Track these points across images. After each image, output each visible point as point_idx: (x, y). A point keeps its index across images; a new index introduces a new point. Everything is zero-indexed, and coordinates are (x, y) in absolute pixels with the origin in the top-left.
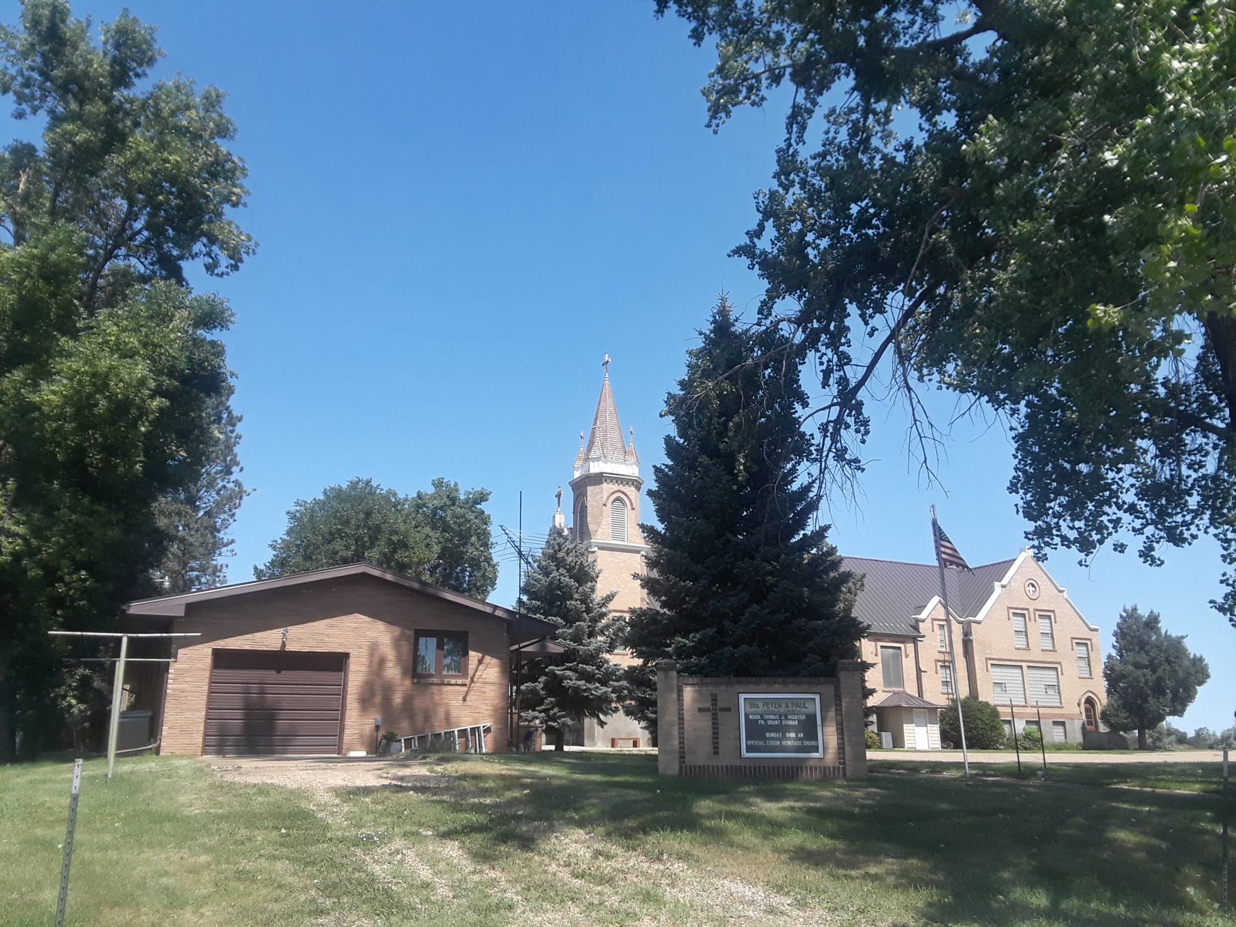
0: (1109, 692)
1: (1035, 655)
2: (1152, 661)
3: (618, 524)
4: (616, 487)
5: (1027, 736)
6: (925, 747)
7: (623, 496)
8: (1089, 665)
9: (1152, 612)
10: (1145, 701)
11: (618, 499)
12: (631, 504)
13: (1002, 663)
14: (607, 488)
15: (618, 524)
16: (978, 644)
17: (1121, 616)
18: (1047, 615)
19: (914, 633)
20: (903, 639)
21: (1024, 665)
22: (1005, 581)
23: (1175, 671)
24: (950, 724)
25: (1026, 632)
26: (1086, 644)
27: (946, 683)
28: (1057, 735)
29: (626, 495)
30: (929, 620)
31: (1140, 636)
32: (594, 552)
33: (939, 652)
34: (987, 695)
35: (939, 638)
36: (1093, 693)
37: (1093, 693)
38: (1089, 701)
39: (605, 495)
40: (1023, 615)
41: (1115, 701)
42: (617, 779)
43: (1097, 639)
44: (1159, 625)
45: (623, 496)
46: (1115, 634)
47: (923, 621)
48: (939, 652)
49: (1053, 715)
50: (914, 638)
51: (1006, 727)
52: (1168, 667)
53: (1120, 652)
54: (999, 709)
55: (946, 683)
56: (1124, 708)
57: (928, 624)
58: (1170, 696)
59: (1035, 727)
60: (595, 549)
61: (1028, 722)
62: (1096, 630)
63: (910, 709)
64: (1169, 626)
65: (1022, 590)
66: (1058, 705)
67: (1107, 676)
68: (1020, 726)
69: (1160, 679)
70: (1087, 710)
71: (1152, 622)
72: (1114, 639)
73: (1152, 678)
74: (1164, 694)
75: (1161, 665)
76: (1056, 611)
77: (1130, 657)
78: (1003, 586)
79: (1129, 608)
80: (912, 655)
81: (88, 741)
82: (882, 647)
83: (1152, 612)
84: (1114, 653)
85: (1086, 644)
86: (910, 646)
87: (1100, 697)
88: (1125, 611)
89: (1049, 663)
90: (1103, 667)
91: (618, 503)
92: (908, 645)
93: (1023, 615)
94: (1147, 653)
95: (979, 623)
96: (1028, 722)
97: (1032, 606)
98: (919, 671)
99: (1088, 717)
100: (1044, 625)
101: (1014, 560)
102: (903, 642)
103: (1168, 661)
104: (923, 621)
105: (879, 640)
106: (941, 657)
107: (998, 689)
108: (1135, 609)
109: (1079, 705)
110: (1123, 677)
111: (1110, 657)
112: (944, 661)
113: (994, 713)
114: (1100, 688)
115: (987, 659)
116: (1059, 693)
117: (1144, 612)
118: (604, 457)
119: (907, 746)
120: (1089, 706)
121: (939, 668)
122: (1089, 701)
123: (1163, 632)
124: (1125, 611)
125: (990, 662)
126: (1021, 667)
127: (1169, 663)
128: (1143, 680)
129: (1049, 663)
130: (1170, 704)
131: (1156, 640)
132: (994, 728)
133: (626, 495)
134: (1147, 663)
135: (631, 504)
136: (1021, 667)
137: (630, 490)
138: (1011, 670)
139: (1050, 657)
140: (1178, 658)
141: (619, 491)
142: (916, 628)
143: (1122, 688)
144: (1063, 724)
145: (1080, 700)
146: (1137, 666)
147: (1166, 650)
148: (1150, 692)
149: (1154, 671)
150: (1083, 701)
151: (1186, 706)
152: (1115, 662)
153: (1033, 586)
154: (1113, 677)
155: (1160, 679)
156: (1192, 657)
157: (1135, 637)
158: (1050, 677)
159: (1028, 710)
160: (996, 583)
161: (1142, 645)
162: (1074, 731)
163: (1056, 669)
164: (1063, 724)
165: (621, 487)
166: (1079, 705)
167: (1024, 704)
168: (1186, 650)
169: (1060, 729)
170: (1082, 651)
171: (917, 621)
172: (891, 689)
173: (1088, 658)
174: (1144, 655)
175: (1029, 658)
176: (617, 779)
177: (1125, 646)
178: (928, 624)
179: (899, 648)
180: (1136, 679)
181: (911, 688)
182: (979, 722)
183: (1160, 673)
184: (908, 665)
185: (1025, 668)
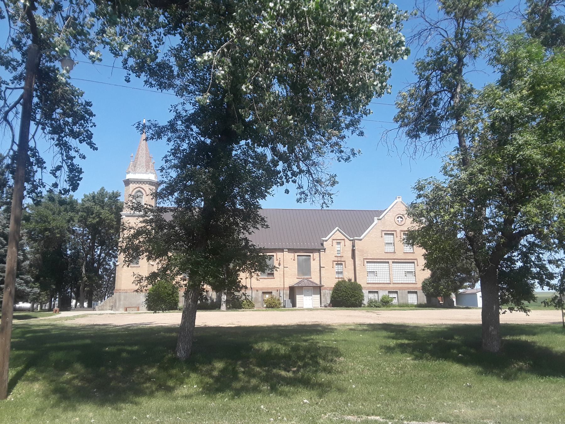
4: (137, 185)
6: (311, 307)
7: (141, 190)
12: (146, 193)
13: (400, 261)
19: (321, 247)
20: (313, 251)
21: (390, 261)
29: (143, 189)
33: (335, 256)
42: (454, 300)
45: (141, 190)
47: (326, 241)
48: (335, 256)
49: (408, 288)
60: (124, 217)
65: (393, 220)
89: (409, 259)
92: (315, 254)
95: (361, 240)
102: (312, 253)
104: (326, 241)
105: (296, 252)
106: (336, 259)
107: (372, 275)
112: (338, 261)
116: (415, 276)
118: (135, 172)
119: (297, 306)
121: (335, 265)
125: (366, 261)
129: (409, 259)
133: (143, 189)
135: (146, 193)
136: (388, 262)
141: (139, 187)
142: (322, 245)
153: (401, 218)
165: (140, 185)
175: (394, 258)
176: (454, 300)
178: (330, 242)
179: (310, 256)
184: (314, 265)
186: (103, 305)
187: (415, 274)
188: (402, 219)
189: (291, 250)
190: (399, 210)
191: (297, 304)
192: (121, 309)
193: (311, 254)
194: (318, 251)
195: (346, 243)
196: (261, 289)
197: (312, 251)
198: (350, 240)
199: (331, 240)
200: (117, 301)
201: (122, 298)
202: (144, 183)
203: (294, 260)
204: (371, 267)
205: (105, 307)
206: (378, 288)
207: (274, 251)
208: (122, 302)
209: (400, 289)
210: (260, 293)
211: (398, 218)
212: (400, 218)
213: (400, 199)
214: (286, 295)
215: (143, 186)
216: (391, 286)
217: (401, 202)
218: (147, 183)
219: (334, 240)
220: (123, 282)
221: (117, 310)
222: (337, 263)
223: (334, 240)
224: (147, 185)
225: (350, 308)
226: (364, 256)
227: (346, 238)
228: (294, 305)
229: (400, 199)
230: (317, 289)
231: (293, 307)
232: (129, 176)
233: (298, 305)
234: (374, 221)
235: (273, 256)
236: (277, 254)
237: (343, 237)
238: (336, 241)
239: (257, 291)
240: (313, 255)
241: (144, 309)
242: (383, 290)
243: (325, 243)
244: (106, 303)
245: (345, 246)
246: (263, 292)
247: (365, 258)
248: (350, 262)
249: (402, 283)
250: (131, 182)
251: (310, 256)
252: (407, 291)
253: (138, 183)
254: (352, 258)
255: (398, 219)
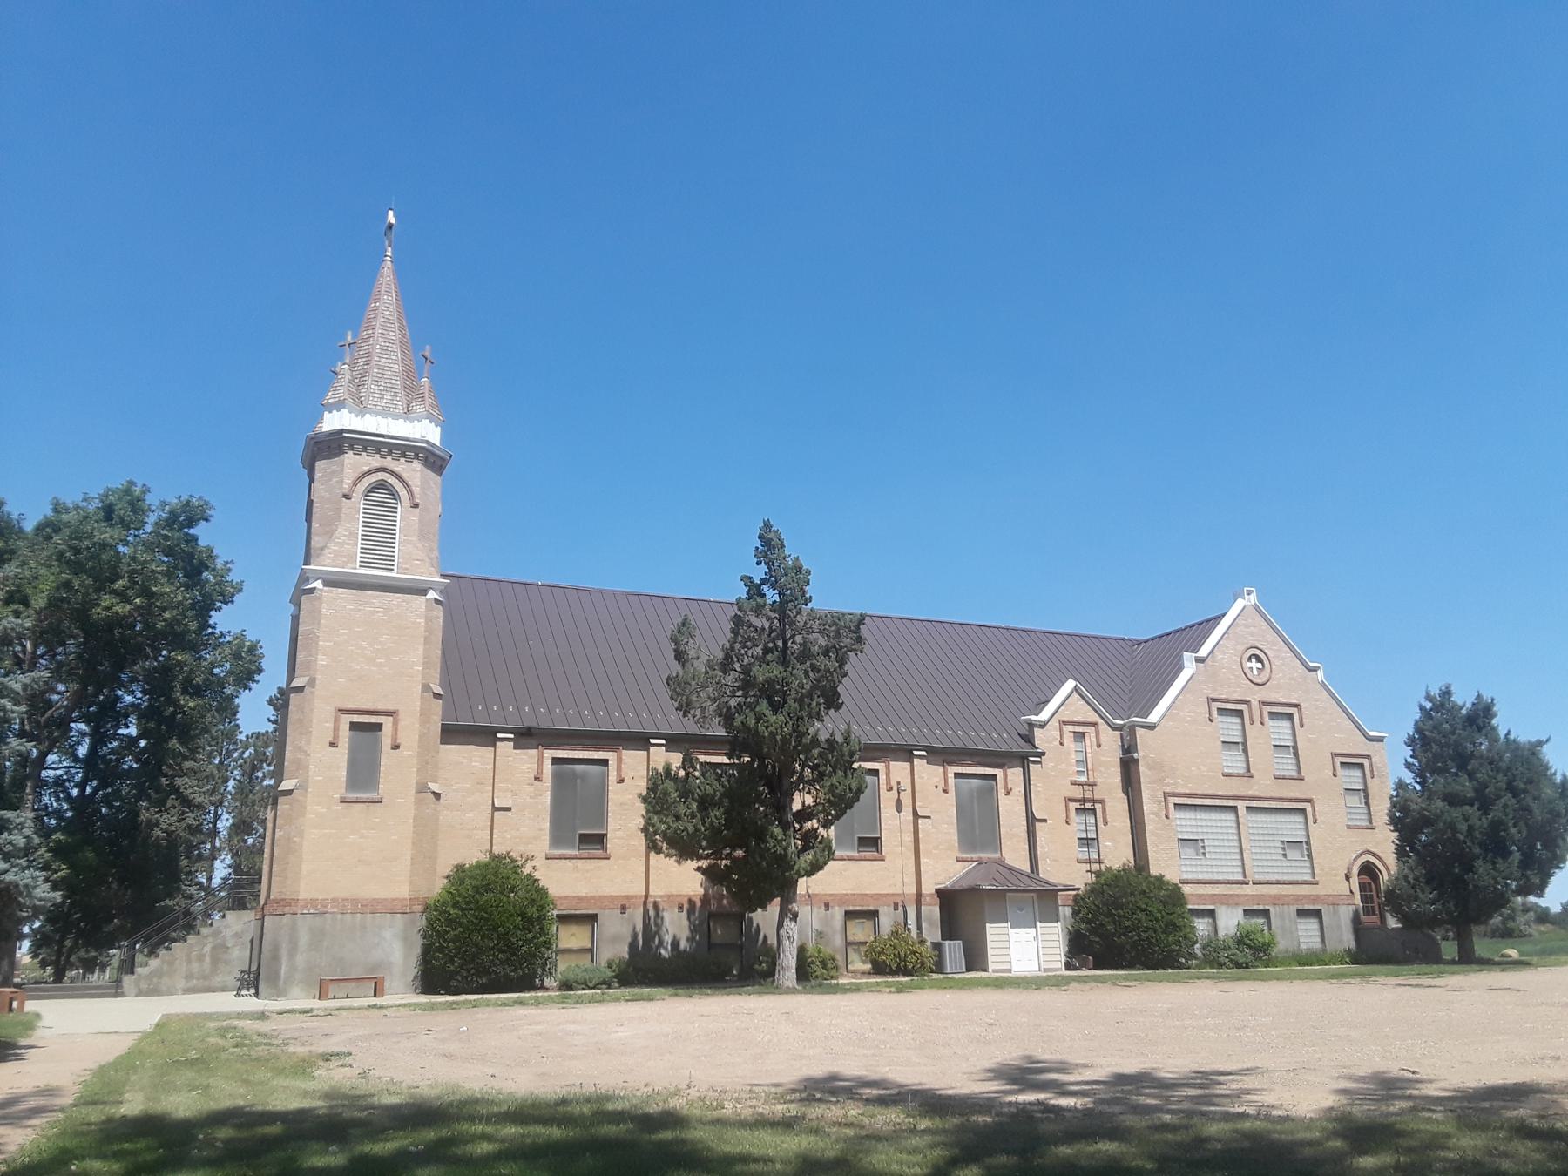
0: (1400, 853)
1: (1263, 785)
2: (1480, 790)
3: (379, 538)
4: (376, 461)
5: (1243, 940)
7: (391, 480)
8: (1367, 804)
9: (1479, 697)
10: (1470, 868)
11: (381, 486)
12: (411, 495)
14: (353, 462)
15: (379, 538)
16: (1150, 768)
17: (1422, 708)
18: (1284, 713)
20: (1001, 759)
21: (1241, 805)
22: (1203, 652)
23: (1528, 810)
24: (1089, 922)
25: (1245, 744)
26: (1361, 766)
27: (1086, 842)
28: (1307, 935)
30: (1055, 723)
31: (1457, 744)
32: (312, 590)
33: (1074, 783)
34: (1167, 864)
35: (1074, 757)
36: (1375, 855)
37: (1375, 855)
38: (1368, 871)
39: (349, 476)
40: (1239, 713)
41: (1411, 869)
43: (1380, 754)
44: (1494, 722)
45: (391, 480)
46: (1411, 742)
47: (1043, 725)
48: (1074, 783)
49: (1298, 898)
50: (1024, 756)
51: (1202, 926)
52: (1514, 801)
53: (1420, 775)
54: (1186, 889)
55: (1086, 842)
56: (1427, 883)
57: (1052, 730)
58: (1516, 857)
59: (1261, 921)
60: (318, 584)
61: (1246, 912)
62: (1380, 740)
63: (999, 895)
64: (1513, 724)
66: (1308, 878)
67: (1396, 823)
68: (1230, 922)
69: (1497, 825)
70: (1362, 887)
71: (1481, 716)
72: (1408, 751)
73: (1481, 822)
74: (1505, 854)
75: (1499, 797)
76: (1303, 705)
77: (1437, 782)
78: (1199, 660)
79: (1435, 692)
80: (1019, 789)
81: (1513, 953)
82: (957, 775)
83: (1479, 697)
84: (1408, 777)
85: (1361, 766)
86: (1015, 774)
87: (1388, 862)
88: (1429, 698)
89: (1290, 800)
90: (1388, 804)
91: (381, 495)
92: (1010, 771)
93: (1239, 713)
94: (1471, 775)
95: (1152, 727)
96: (1246, 912)
97: (1256, 696)
98: (1031, 820)
99: (1364, 899)
100: (1279, 731)
101: (1224, 615)
103: (1512, 789)
105: (950, 763)
106: (1077, 792)
107: (1189, 852)
108: (1447, 693)
109: (1348, 877)
110: (1425, 822)
111: (1400, 785)
112: (1083, 801)
113: (1174, 896)
114: (1384, 844)
115: (1167, 795)
116: (1310, 856)
117: (1464, 698)
119: (991, 966)
120: (1367, 879)
121: (1073, 813)
122: (1368, 871)
123: (1502, 734)
124: (1429, 698)
126: (1234, 809)
127: (1512, 789)
128: (1463, 827)
129: (1290, 800)
130: (1517, 874)
131: (1489, 750)
132: (1172, 927)
134: (1471, 794)
135: (411, 495)
136: (1234, 809)
137: (413, 471)
138: (1214, 816)
139: (1292, 791)
140: (1530, 782)
141: (384, 469)
142: (1029, 739)
143: (1425, 846)
144: (1317, 914)
145: (1349, 869)
146: (1452, 800)
147: (1509, 768)
148: (1477, 851)
149: (1485, 809)
150: (1355, 870)
151: (1550, 875)
152: (1414, 796)
153: (1259, 660)
154: (1406, 821)
155: (1497, 825)
156: (1558, 779)
157: (1447, 745)
158: (1291, 826)
159: (1249, 890)
160: (1186, 655)
161: (1463, 760)
162: (1339, 927)
163: (1303, 811)
164: (1317, 914)
165: (389, 462)
166: (1348, 877)
167: (1240, 877)
168: (1547, 768)
169: (1312, 924)
170: (1353, 778)
171: (1031, 725)
172: (975, 856)
173: (1365, 791)
174: (1464, 777)
175: (1251, 793)
177: (1427, 763)
178: (1052, 730)
179: (994, 777)
180: (1452, 827)
181: (1015, 854)
182: (1142, 916)
183: (1496, 813)
184: (1010, 810)
185: (1242, 811)
186: (158, 973)
187: (1309, 849)
188: (1260, 665)
189: (940, 755)
190: (1252, 634)
191: (991, 959)
192: (296, 991)
193: (998, 772)
194: (1019, 762)
195: (1103, 738)
196: (842, 899)
197: (1000, 761)
198: (1115, 728)
199: (1055, 723)
200: (284, 953)
201: (304, 939)
202: (403, 455)
203: (945, 791)
204: (1187, 823)
205: (165, 980)
206: (1214, 898)
207: (877, 754)
208: (300, 959)
209: (1278, 900)
210: (838, 914)
211: (1250, 659)
212: (1254, 660)
213: (1253, 599)
214: (931, 923)
215: (401, 466)
216: (1249, 890)
217: (1256, 608)
218: (417, 457)
219: (1065, 723)
220: (305, 868)
221: (280, 993)
222: (1077, 805)
223: (1065, 723)
224: (416, 465)
225: (1161, 972)
226: (1168, 785)
227: (1101, 721)
228: (975, 958)
229: (1253, 599)
230: (1042, 900)
231: (968, 970)
232: (332, 422)
233: (994, 962)
234: (1181, 668)
235: (875, 772)
236: (888, 768)
237: (1094, 717)
238: (1070, 728)
239: (827, 906)
240: (1005, 776)
241: (401, 994)
242: (1228, 905)
243: (1038, 732)
244: (171, 963)
245: (1099, 746)
246: (1298, 910)
247: (1168, 790)
248: (1117, 805)
249: (1278, 883)
250: (352, 444)
251: (994, 777)
252: (1293, 909)
253: (378, 451)
254: (1126, 792)
255: (1249, 665)
